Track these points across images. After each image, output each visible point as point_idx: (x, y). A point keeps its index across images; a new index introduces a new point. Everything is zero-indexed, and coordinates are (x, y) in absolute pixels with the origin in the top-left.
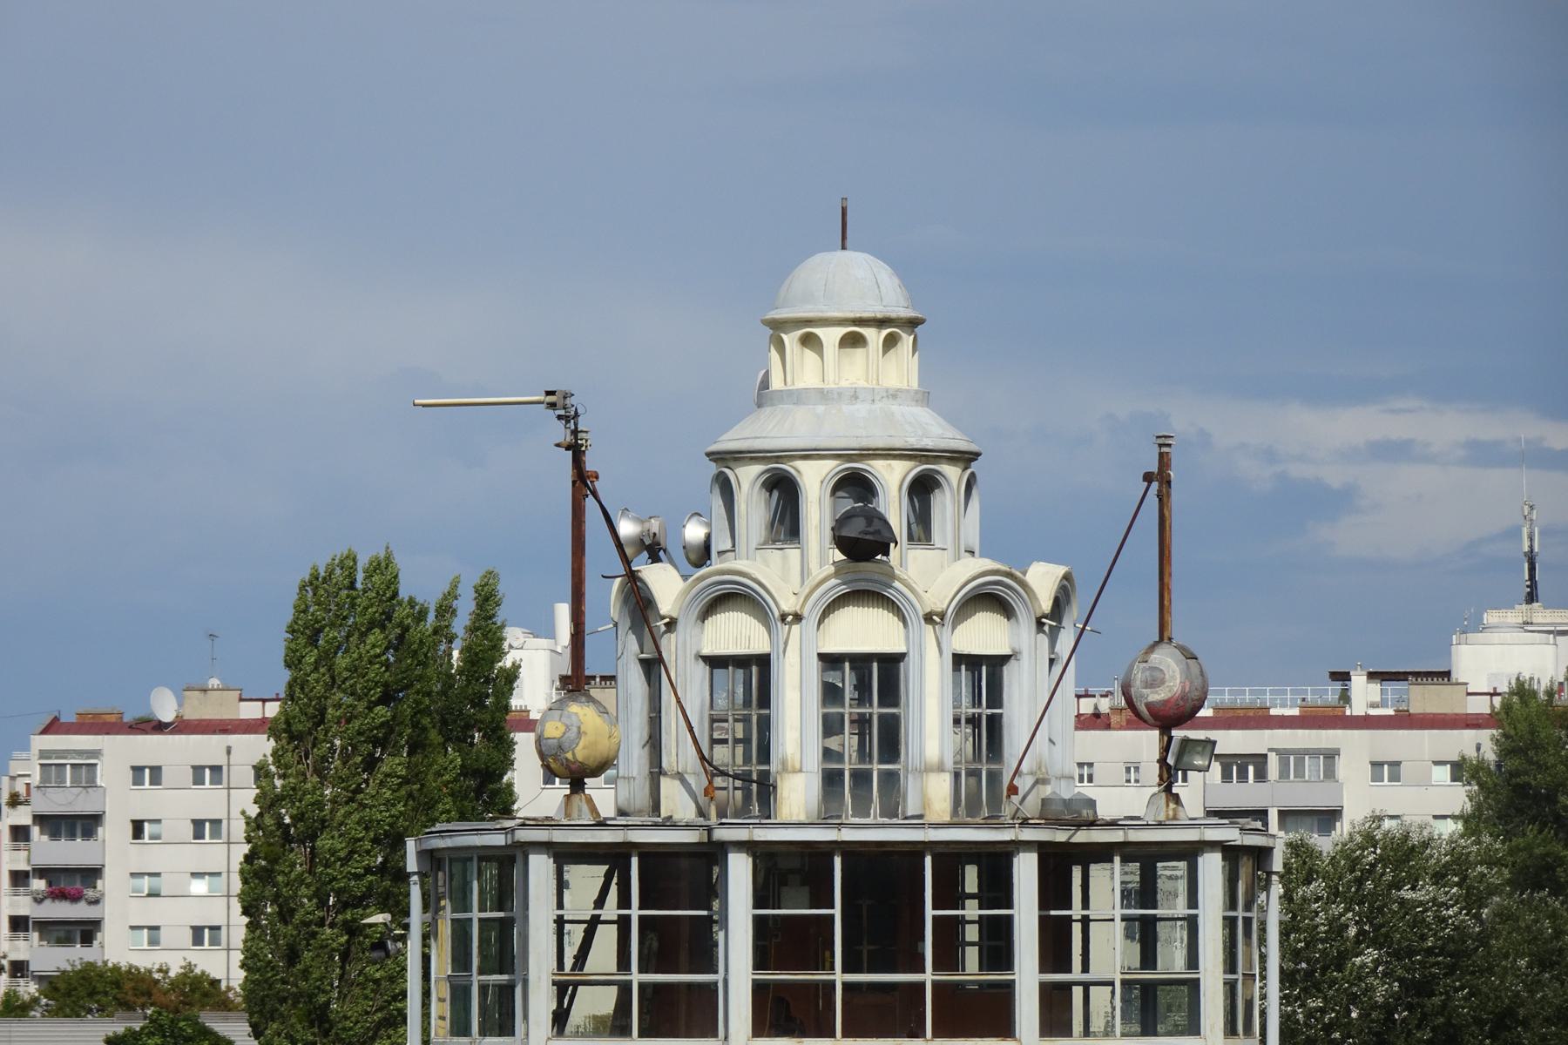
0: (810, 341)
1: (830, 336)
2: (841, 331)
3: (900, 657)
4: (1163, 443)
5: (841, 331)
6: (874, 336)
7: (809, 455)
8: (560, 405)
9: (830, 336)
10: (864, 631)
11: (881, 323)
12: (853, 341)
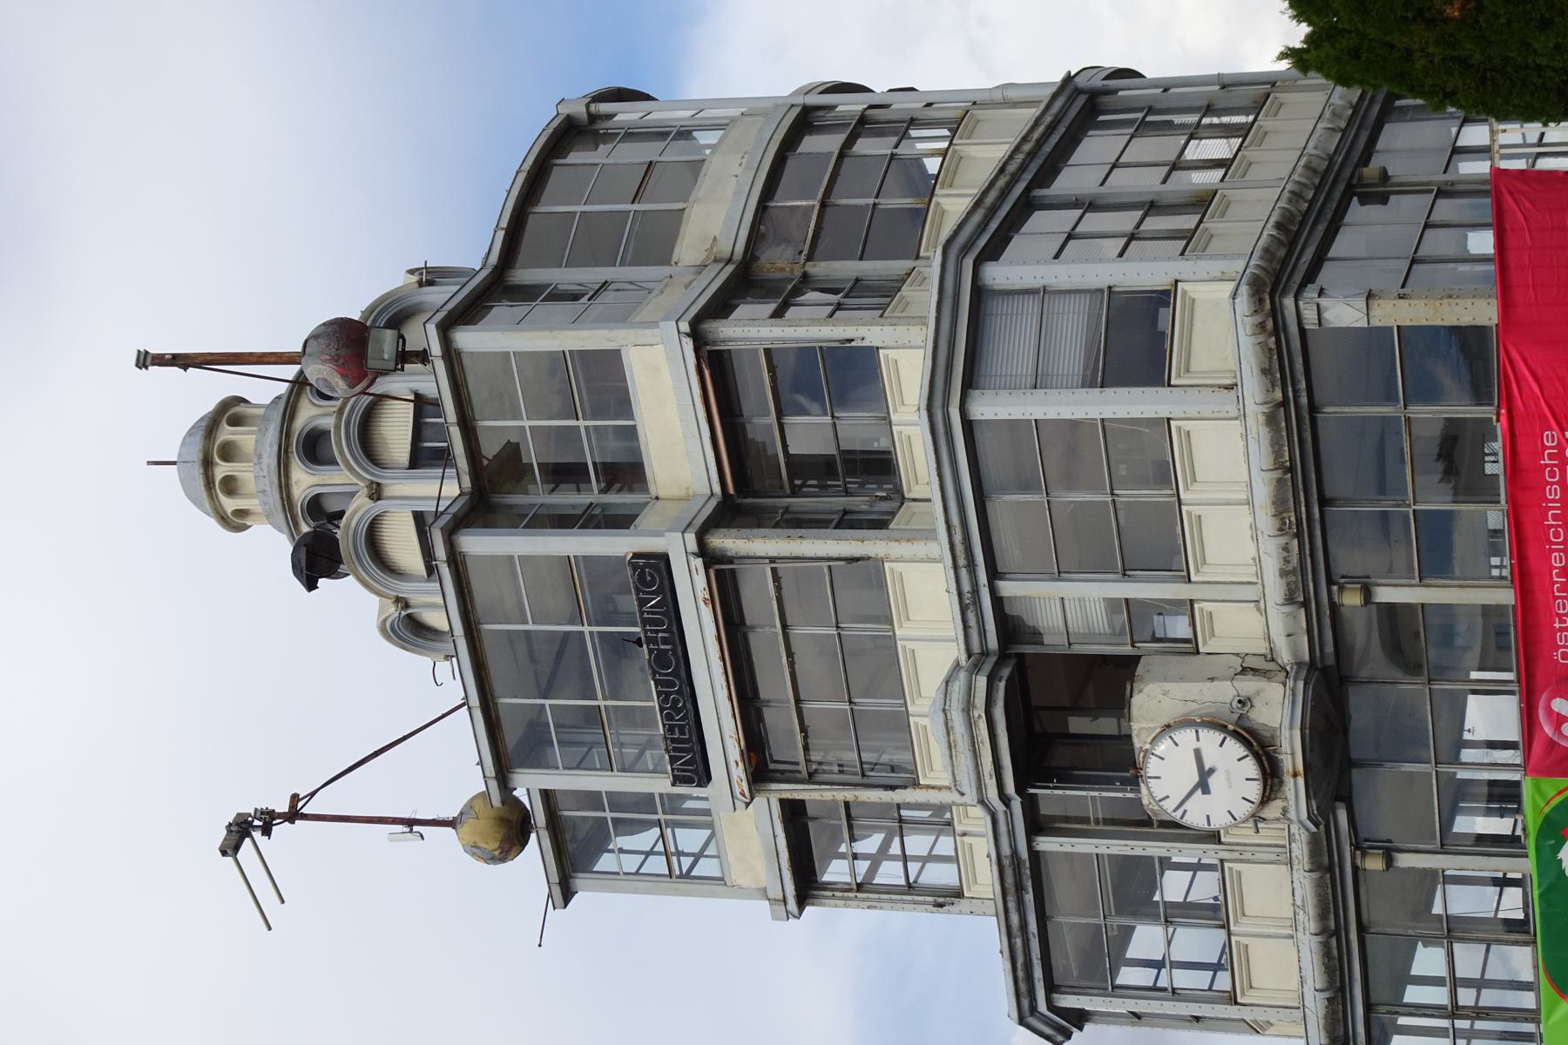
2: (223, 499)
4: (145, 360)
5: (223, 499)
6: (222, 470)
8: (240, 830)
11: (207, 464)
12: (230, 485)
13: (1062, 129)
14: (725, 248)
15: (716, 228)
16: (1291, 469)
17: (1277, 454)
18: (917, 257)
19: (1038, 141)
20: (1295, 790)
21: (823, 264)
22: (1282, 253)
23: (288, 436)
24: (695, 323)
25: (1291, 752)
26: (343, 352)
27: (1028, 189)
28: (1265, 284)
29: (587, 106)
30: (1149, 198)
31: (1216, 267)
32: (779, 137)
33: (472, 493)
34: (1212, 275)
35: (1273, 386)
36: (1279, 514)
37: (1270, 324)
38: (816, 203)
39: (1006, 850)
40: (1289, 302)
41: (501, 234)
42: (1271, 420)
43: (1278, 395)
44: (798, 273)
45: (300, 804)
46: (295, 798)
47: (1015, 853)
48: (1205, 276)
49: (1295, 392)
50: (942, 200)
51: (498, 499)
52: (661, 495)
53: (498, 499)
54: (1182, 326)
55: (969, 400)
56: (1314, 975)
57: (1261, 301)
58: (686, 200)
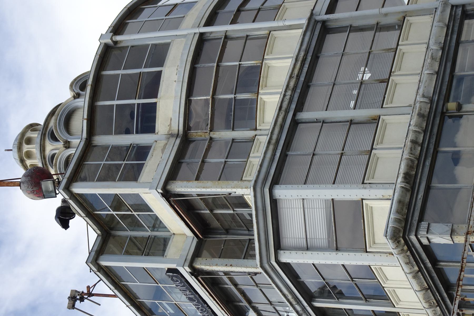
13: (310, 54)
14: (175, 128)
15: (170, 114)
16: (430, 288)
17: (420, 284)
18: (256, 129)
19: (297, 76)
21: (217, 133)
22: (407, 199)
23: (45, 158)
24: (164, 188)
26: (35, 189)
27: (294, 115)
28: (400, 231)
29: (111, 39)
30: (349, 119)
31: (380, 192)
32: (190, 59)
33: (102, 235)
34: (378, 197)
35: (413, 266)
37: (406, 248)
38: (209, 97)
40: (413, 238)
41: (85, 122)
43: (416, 268)
44: (208, 137)
45: (91, 290)
46: (88, 288)
48: (375, 197)
49: (453, 26)
50: (263, 97)
51: (114, 232)
52: (175, 233)
53: (114, 232)
54: (368, 221)
55: (279, 255)
57: (399, 242)
58: (156, 97)
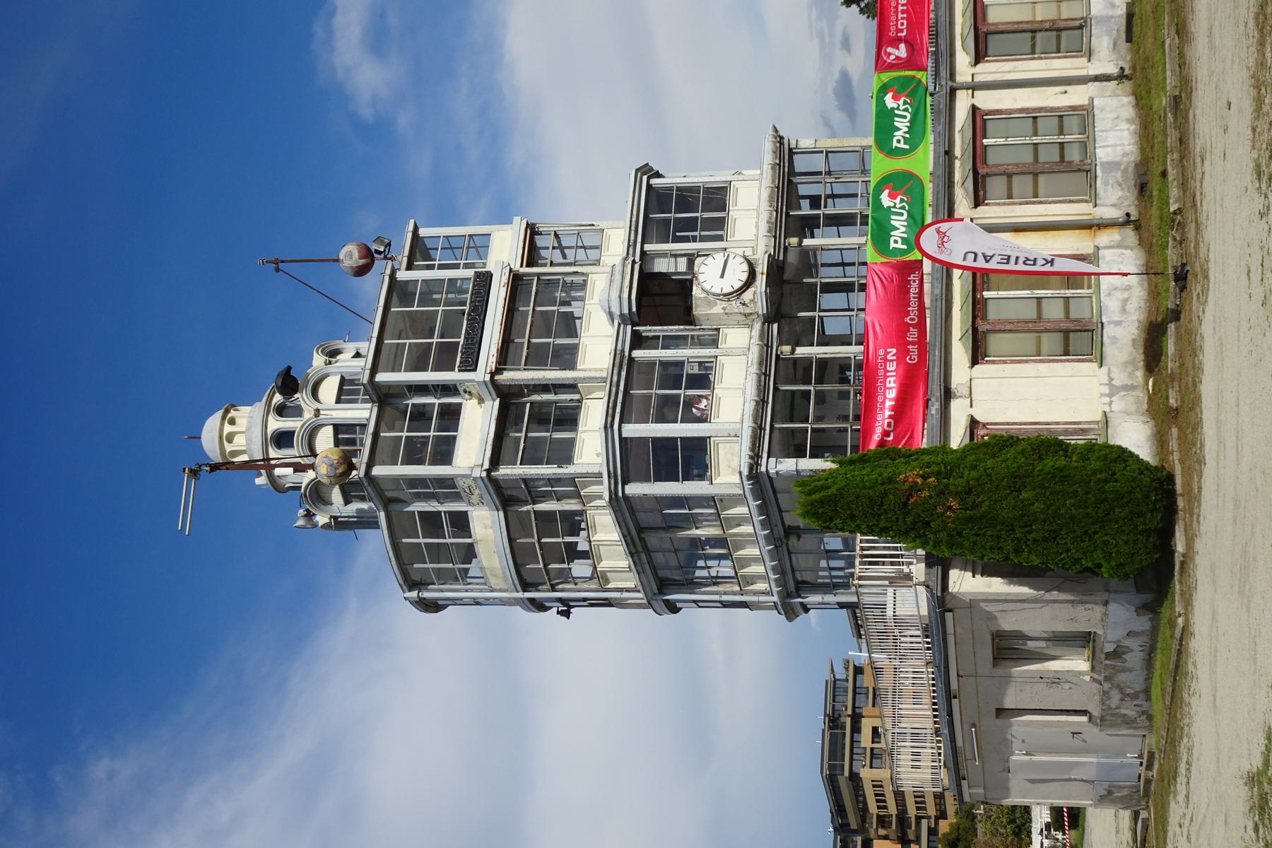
0: (230, 438)
1: (228, 428)
3: (342, 377)
7: (265, 425)
9: (228, 428)
10: (329, 390)
12: (232, 422)
20: (761, 281)
25: (762, 268)
36: (771, 201)
39: (619, 347)
42: (773, 168)
47: (623, 351)
56: (750, 407)
